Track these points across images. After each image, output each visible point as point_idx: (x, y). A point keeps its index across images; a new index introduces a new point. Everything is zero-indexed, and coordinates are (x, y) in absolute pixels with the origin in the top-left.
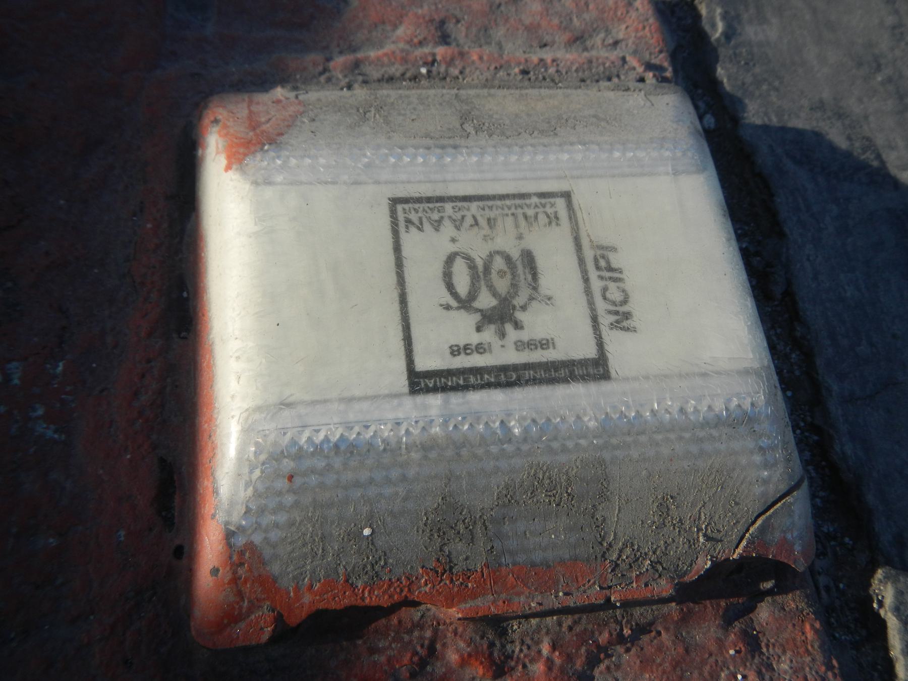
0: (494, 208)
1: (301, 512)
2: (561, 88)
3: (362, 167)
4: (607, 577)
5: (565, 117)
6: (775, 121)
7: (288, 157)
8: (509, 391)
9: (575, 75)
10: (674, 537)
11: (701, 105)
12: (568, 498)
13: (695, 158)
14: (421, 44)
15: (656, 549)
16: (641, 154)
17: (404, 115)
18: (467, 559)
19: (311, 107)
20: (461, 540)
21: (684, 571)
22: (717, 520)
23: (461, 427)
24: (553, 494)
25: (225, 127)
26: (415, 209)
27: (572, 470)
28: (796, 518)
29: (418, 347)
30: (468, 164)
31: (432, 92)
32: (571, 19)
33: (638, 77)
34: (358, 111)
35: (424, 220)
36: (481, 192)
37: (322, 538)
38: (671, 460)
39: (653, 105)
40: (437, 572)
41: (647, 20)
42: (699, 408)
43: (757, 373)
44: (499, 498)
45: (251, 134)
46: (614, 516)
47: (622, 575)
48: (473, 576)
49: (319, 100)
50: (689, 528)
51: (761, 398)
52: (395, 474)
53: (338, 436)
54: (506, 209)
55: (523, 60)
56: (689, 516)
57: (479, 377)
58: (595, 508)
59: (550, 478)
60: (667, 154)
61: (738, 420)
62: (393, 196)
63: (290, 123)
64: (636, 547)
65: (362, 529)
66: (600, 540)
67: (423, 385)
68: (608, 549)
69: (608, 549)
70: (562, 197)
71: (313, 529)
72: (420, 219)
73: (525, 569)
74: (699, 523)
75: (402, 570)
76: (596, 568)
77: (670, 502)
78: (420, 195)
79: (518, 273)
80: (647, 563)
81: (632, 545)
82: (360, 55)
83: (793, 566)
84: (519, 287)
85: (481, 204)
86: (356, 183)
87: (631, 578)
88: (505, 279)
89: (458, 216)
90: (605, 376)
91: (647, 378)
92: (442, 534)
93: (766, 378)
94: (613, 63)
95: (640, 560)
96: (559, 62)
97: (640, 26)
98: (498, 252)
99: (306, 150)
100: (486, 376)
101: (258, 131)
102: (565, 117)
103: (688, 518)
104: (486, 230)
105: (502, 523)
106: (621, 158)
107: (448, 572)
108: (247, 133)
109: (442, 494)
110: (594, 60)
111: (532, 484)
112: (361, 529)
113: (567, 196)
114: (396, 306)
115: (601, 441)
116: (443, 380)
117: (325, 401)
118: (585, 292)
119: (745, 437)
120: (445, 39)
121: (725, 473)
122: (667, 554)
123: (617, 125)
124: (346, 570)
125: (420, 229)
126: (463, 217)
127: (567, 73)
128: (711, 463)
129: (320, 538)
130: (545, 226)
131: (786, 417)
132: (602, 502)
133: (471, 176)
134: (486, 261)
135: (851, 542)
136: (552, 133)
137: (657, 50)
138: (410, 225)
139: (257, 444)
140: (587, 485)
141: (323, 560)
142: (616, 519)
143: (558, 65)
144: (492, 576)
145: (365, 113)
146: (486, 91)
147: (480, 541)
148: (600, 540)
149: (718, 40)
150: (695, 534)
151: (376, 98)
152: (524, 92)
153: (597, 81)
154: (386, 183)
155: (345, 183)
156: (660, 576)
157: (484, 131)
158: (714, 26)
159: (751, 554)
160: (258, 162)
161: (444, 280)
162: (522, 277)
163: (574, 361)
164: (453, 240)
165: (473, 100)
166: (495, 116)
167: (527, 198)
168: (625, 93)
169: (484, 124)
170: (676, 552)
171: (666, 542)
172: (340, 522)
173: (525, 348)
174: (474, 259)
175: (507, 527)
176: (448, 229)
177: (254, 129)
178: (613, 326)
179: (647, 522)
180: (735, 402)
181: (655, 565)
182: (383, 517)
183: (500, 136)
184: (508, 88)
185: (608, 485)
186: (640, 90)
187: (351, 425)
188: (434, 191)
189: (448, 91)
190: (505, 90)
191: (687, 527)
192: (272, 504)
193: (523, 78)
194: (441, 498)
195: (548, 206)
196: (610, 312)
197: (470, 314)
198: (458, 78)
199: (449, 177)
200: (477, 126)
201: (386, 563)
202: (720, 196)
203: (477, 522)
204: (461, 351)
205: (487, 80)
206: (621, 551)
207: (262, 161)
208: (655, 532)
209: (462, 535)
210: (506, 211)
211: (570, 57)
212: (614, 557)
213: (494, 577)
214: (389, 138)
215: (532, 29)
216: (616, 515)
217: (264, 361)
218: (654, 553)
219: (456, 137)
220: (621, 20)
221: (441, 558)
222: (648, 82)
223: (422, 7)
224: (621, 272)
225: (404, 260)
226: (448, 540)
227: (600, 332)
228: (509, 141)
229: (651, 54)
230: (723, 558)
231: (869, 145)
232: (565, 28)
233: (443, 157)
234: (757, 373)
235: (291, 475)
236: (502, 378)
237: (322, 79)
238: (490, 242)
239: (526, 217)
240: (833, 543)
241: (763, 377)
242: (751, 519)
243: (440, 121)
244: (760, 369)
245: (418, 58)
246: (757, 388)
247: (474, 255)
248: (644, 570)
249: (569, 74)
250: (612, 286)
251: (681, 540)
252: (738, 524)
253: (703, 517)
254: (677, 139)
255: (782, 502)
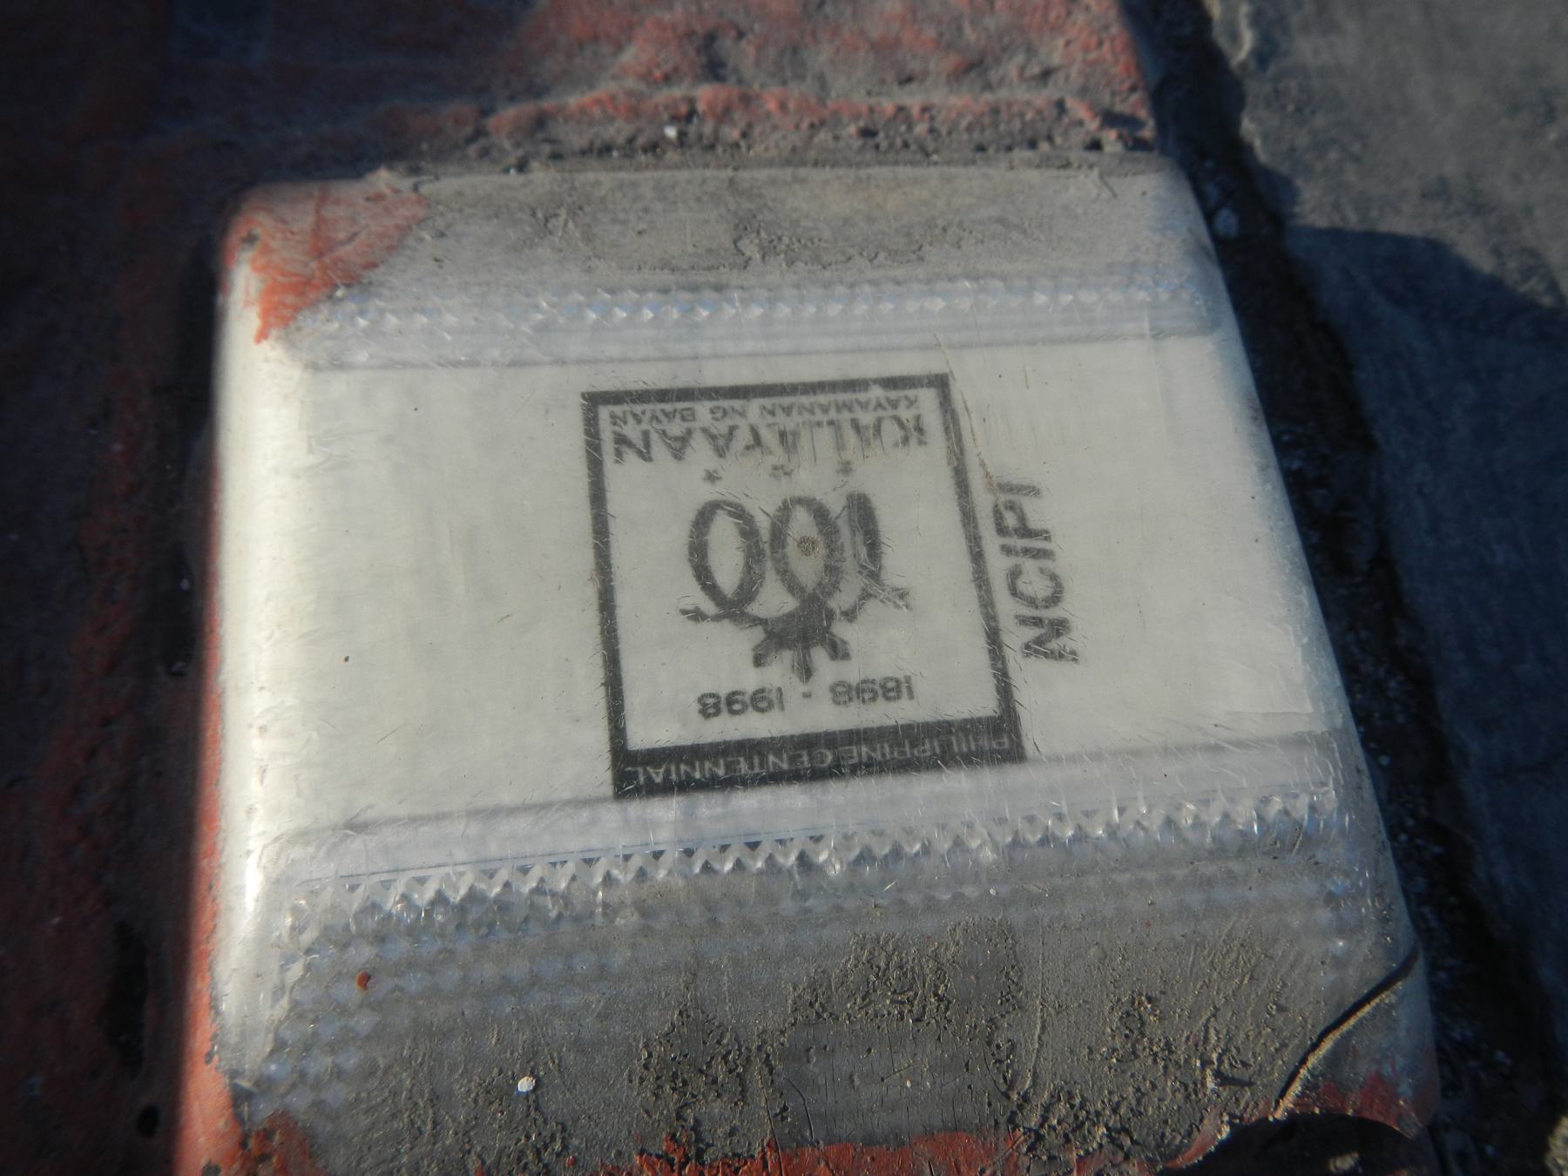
0: (795, 412)
1: (388, 1048)
2: (936, 163)
3: (529, 332)
4: (1020, 1162)
5: (940, 222)
6: (1353, 221)
7: (382, 312)
8: (817, 789)
9: (965, 136)
10: (1155, 1079)
11: (1212, 190)
12: (939, 1006)
13: (1197, 303)
14: (667, 79)
15: (1118, 1104)
16: (1089, 297)
17: (624, 222)
18: (732, 1132)
19: (441, 208)
20: (719, 1095)
21: (1176, 1146)
22: (1242, 1043)
23: (717, 866)
24: (908, 999)
25: (266, 250)
26: (635, 415)
27: (947, 949)
28: (1402, 1034)
29: (634, 700)
30: (743, 321)
31: (682, 175)
32: (960, 29)
33: (1088, 140)
34: (534, 214)
35: (654, 437)
36: (769, 378)
37: (432, 1101)
38: (1148, 925)
39: (1115, 195)
40: (671, 1162)
41: (1106, 28)
42: (1204, 817)
43: (1321, 743)
44: (796, 1009)
45: (314, 265)
46: (1033, 1039)
47: (1051, 1158)
48: (746, 1167)
49: (460, 194)
50: (1186, 1060)
51: (1330, 798)
52: (583, 965)
53: (463, 891)
54: (818, 411)
55: (864, 109)
56: (1185, 1035)
57: (756, 761)
58: (994, 1024)
59: (901, 967)
60: (1142, 296)
61: (1283, 842)
62: (591, 389)
63: (395, 244)
64: (1077, 1101)
65: (515, 1078)
66: (1003, 1088)
67: (642, 779)
68: (1020, 1107)
69: (1020, 1107)
70: (933, 386)
71: (413, 1081)
72: (646, 435)
73: (852, 1151)
74: (1206, 1049)
75: (598, 1160)
76: (996, 1145)
77: (1146, 1008)
78: (644, 387)
79: (839, 543)
80: (1100, 1133)
81: (1070, 1096)
82: (547, 104)
83: (1397, 1129)
84: (842, 572)
85: (768, 402)
86: (517, 363)
87: (1067, 1163)
88: (812, 556)
89: (721, 427)
90: (1015, 754)
91: (1097, 756)
92: (684, 1088)
93: (1340, 754)
94: (1039, 112)
95: (1087, 1125)
96: (934, 112)
97: (1093, 41)
98: (799, 501)
99: (418, 299)
100: (771, 758)
101: (327, 260)
102: (940, 222)
103: (1184, 1039)
104: (778, 456)
105: (805, 1059)
106: (1048, 307)
107: (694, 1161)
108: (306, 265)
109: (680, 1003)
110: (1003, 108)
111: (865, 979)
112: (513, 1078)
113: (941, 383)
114: (592, 617)
115: (1005, 890)
116: (683, 767)
117: (439, 817)
118: (975, 581)
119: (1298, 876)
120: (714, 69)
121: (1258, 949)
122: (1141, 1113)
123: (1042, 238)
124: (483, 1162)
125: (646, 456)
126: (732, 429)
127: (949, 133)
128: (1229, 928)
129: (428, 1099)
130: (896, 445)
131: (1380, 832)
132: (1008, 1012)
133: (749, 345)
134: (775, 520)
135: (1508, 1062)
136: (913, 257)
137: (1127, 85)
138: (625, 449)
139: (296, 910)
140: (977, 978)
141: (434, 1144)
142: (1037, 1046)
143: (932, 119)
144: (785, 1167)
145: (547, 220)
146: (788, 173)
147: (759, 1096)
148: (1003, 1088)
149: (1243, 65)
150: (1198, 1072)
151: (573, 188)
152: (864, 172)
153: (1009, 149)
154: (580, 361)
155: (494, 364)
156: (1127, 1158)
157: (778, 255)
158: (1235, 37)
159: (1311, 1109)
160: (321, 323)
161: (690, 561)
162: (848, 552)
163: (950, 724)
164: (711, 477)
165: (763, 191)
166: (804, 223)
167: (860, 391)
168: (1062, 173)
169: (780, 239)
170: (1159, 1108)
171: (1138, 1090)
172: (469, 1066)
173: (851, 699)
174: (751, 516)
175: (814, 1067)
176: (701, 454)
177: (319, 254)
178: (1034, 648)
179: (1099, 1049)
180: (1277, 804)
181: (1117, 1136)
182: (559, 1054)
183: (809, 265)
184: (833, 166)
185: (1019, 977)
186: (1091, 167)
187: (488, 866)
188: (675, 377)
189: (716, 173)
190: (827, 168)
191: (1182, 1058)
192: (329, 1032)
193: (864, 145)
194: (677, 1012)
195: (903, 404)
196: (1024, 621)
197: (741, 629)
198: (737, 145)
199: (705, 348)
200: (766, 244)
201: (565, 1147)
202: (1245, 378)
203: (752, 1058)
204: (723, 705)
205: (794, 149)
206: (1047, 1109)
207: (328, 321)
208: (1116, 1070)
209: (722, 1085)
210: (819, 416)
211: (956, 102)
212: (1034, 1121)
213: (789, 1168)
214: (589, 270)
215: (884, 49)
216: (1037, 1037)
217: (315, 735)
218: (1115, 1111)
219: (721, 268)
220: (1056, 29)
221: (678, 1134)
222: (1108, 149)
223: (670, 7)
224: (1047, 539)
225: (610, 520)
226: (694, 1096)
227: (1004, 663)
228: (827, 274)
229: (1113, 94)
230: (1253, 1119)
231: (1535, 263)
232: (949, 46)
233: (692, 309)
234: (1321, 743)
235: (366, 974)
236: (802, 762)
237: (472, 150)
238: (784, 479)
239: (856, 425)
240: (1473, 1063)
241: (1332, 750)
242: (1311, 1039)
243: (693, 234)
244: (1327, 734)
245: (661, 108)
246: (1321, 774)
247: (752, 507)
248: (1095, 1145)
249: (954, 135)
250: (1030, 566)
251: (1169, 1084)
252: (1283, 1049)
253: (1213, 1038)
254: (1160, 266)
255: (1373, 1003)
